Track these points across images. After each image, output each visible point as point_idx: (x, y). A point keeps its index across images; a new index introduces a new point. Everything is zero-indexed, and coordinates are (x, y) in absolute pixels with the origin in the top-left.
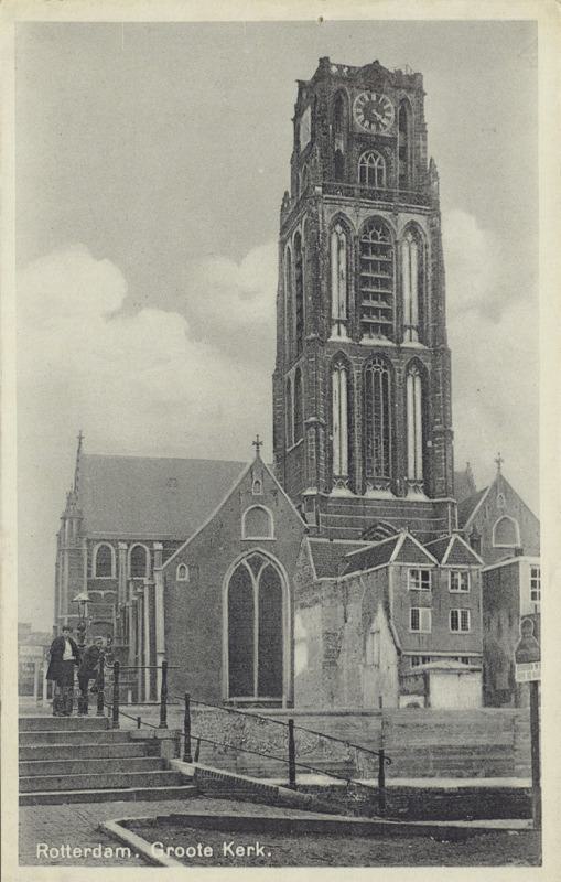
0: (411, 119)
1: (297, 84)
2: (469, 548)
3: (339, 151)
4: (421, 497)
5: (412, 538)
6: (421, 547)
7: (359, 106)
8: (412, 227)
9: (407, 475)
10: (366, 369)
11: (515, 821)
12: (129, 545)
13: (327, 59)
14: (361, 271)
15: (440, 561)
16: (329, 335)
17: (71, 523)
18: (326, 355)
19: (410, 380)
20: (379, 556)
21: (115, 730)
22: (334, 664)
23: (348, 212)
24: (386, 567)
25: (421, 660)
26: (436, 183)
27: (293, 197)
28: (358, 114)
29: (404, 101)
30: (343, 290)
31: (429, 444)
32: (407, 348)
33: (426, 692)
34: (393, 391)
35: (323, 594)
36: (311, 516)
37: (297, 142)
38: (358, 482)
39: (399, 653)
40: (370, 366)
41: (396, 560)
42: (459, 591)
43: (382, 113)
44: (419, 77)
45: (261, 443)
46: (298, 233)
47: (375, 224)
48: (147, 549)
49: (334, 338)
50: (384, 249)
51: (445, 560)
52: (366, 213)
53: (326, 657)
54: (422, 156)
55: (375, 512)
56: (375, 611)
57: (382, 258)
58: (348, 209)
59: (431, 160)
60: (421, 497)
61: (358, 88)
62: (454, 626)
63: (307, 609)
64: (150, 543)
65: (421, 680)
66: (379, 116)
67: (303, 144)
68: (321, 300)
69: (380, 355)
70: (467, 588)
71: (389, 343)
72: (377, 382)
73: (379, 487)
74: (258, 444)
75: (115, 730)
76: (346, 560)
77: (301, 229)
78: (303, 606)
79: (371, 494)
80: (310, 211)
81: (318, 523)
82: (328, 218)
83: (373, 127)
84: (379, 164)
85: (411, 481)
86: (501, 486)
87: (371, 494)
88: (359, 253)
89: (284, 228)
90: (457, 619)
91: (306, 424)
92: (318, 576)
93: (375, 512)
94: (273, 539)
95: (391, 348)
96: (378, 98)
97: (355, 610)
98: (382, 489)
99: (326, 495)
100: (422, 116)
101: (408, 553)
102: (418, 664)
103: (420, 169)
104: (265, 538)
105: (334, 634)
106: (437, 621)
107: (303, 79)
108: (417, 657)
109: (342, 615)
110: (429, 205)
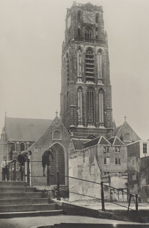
0: (100, 19)
1: (67, 9)
2: (120, 140)
3: (79, 28)
4: (103, 128)
5: (104, 137)
6: (107, 140)
7: (84, 15)
8: (100, 51)
9: (99, 122)
10: (87, 91)
11: (105, 220)
12: (20, 143)
13: (75, 2)
14: (86, 63)
15: (112, 144)
16: (77, 81)
17: (4, 136)
18: (77, 87)
19: (100, 94)
20: (96, 142)
21: (28, 187)
22: (81, 174)
23: (82, 46)
24: (97, 146)
25: (107, 173)
26: (107, 38)
27: (65, 42)
28: (85, 18)
29: (97, 14)
30: (81, 68)
31: (105, 112)
32: (99, 85)
33: (109, 182)
34: (95, 97)
35: (77, 155)
36: (72, 133)
37: (67, 27)
38: (86, 123)
39: (101, 171)
40: (88, 90)
41: (100, 144)
42: (118, 153)
43: (91, 17)
44: (101, 7)
45: (58, 112)
46: (67, 53)
47: (89, 49)
48: (25, 144)
49: (78, 82)
50: (92, 57)
51: (113, 144)
52: (87, 46)
53: (78, 173)
54: (103, 30)
55: (90, 132)
56: (93, 159)
57: (91, 59)
58: (82, 45)
59: (105, 31)
60: (103, 128)
61: (84, 10)
62: (116, 163)
63: (72, 159)
64: (26, 142)
65: (108, 179)
66: (90, 18)
67: (69, 27)
68: (75, 71)
69: (91, 87)
70: (120, 152)
71: (94, 84)
72: (90, 95)
73: (91, 125)
74: (57, 113)
75: (28, 187)
76: (83, 145)
77: (68, 51)
78: (71, 158)
79: (89, 127)
80: (71, 46)
81: (74, 135)
82: (76, 48)
83: (89, 21)
84: (91, 32)
85: (101, 123)
86: (126, 126)
87: (89, 127)
88: (85, 58)
89: (63, 51)
90: (117, 161)
91: (70, 107)
92: (76, 149)
93: (90, 132)
94: (61, 140)
95: (95, 85)
96: (90, 13)
97: (87, 159)
98: (92, 125)
99: (76, 127)
100: (103, 18)
101: (103, 142)
102: (106, 174)
103: (102, 34)
104: (59, 140)
105: (80, 166)
106: (111, 162)
107: (68, 8)
108: (106, 172)
109: (83, 160)
110: (105, 44)
